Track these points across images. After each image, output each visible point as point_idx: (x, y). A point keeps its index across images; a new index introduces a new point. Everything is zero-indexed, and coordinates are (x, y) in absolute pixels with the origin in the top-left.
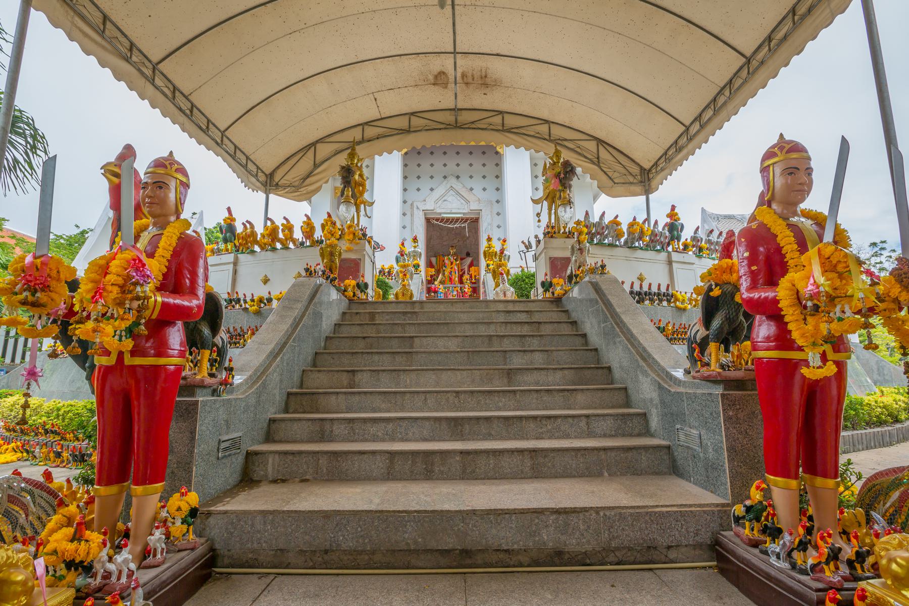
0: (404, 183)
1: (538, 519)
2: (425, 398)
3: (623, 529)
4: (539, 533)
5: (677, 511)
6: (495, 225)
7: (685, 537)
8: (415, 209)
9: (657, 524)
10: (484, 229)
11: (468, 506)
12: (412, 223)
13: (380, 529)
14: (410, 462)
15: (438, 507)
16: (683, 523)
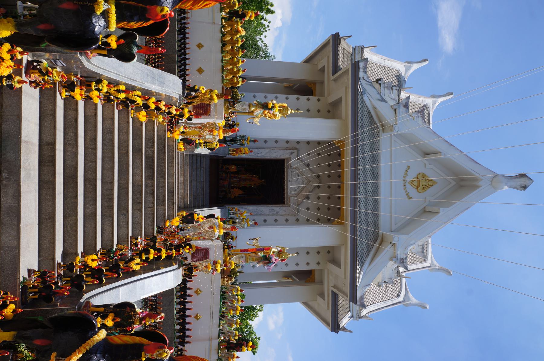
0: (304, 142)
1: (15, 216)
2: (93, 162)
3: (9, 257)
4: (8, 216)
5: (17, 283)
6: (277, 218)
7: (4, 286)
8: (291, 151)
9: (11, 273)
10: (273, 208)
11: (23, 183)
12: (280, 148)
13: (12, 142)
14: (49, 154)
15: (22, 169)
16: (11, 286)
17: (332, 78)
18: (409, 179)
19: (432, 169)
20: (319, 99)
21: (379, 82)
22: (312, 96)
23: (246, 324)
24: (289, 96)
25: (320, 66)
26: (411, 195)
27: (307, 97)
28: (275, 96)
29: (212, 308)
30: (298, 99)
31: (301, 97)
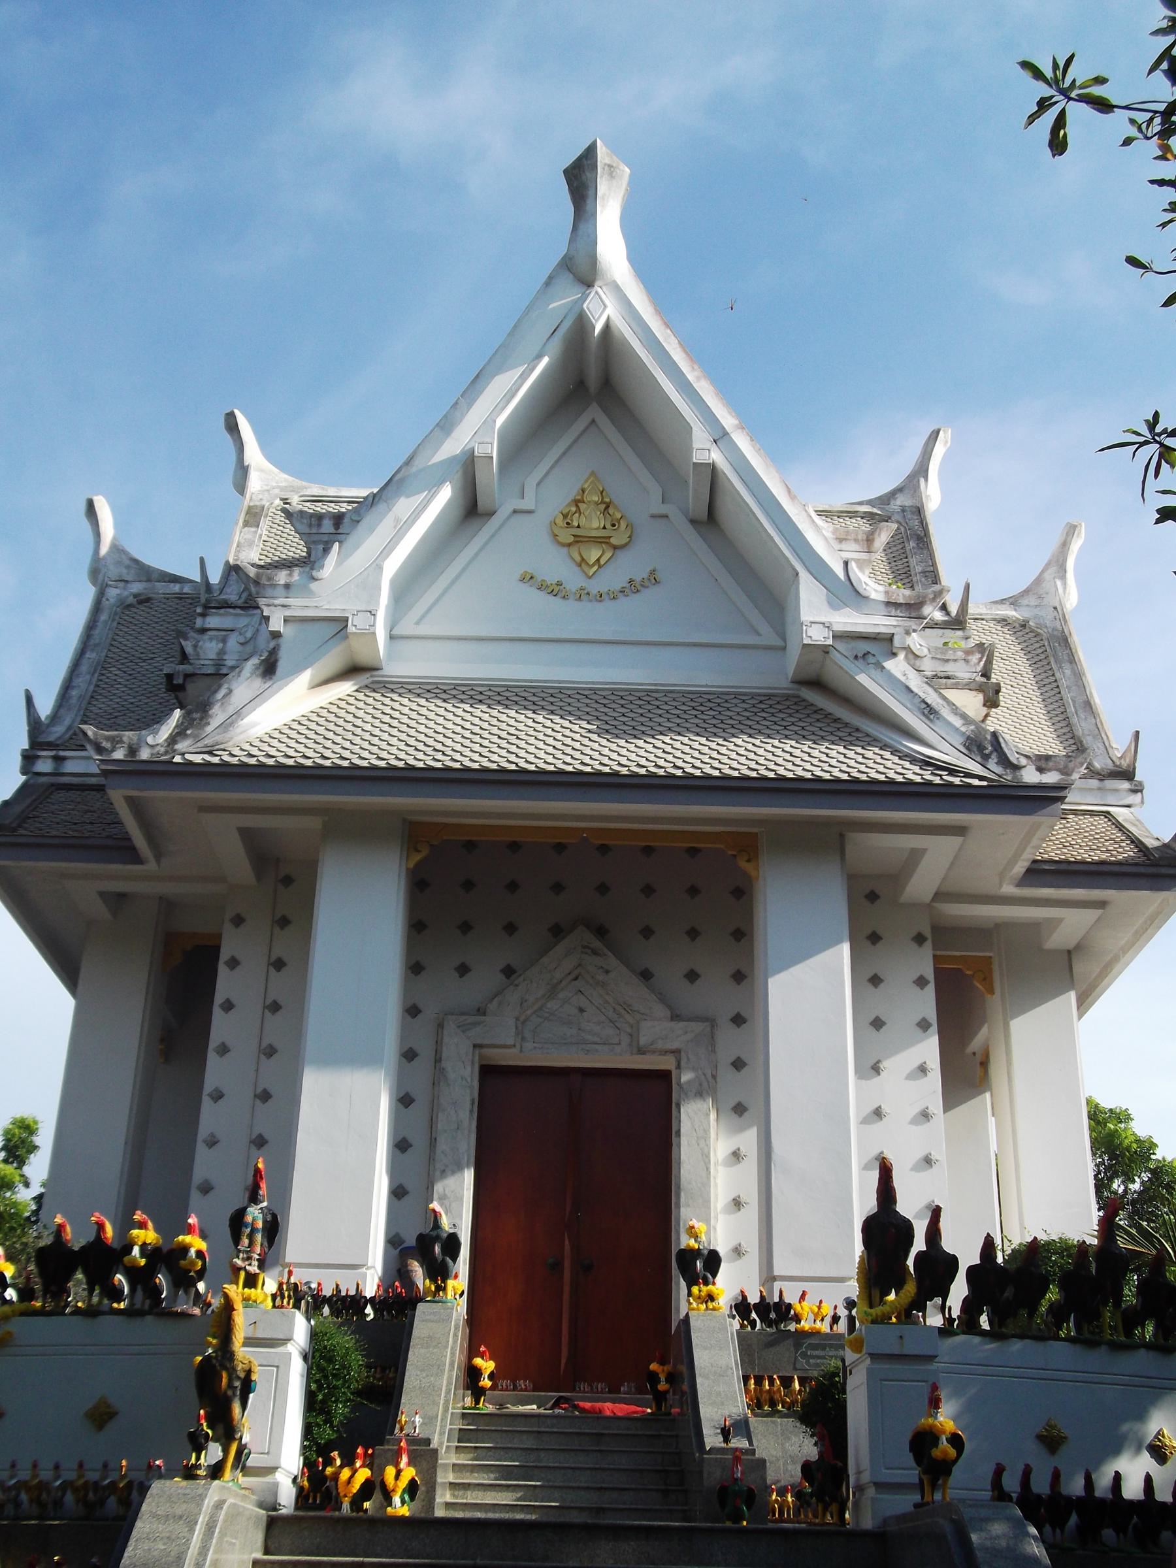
0: (407, 988)
17: (151, 866)
18: (573, 579)
19: (538, 484)
20: (222, 1006)
21: (180, 681)
22: (217, 949)
23: (601, 489)
24: (215, 1040)
25: (101, 911)
26: (640, 575)
27: (222, 970)
28: (211, 1102)
29: (581, 539)
30: (223, 1050)
31: (205, 1128)
